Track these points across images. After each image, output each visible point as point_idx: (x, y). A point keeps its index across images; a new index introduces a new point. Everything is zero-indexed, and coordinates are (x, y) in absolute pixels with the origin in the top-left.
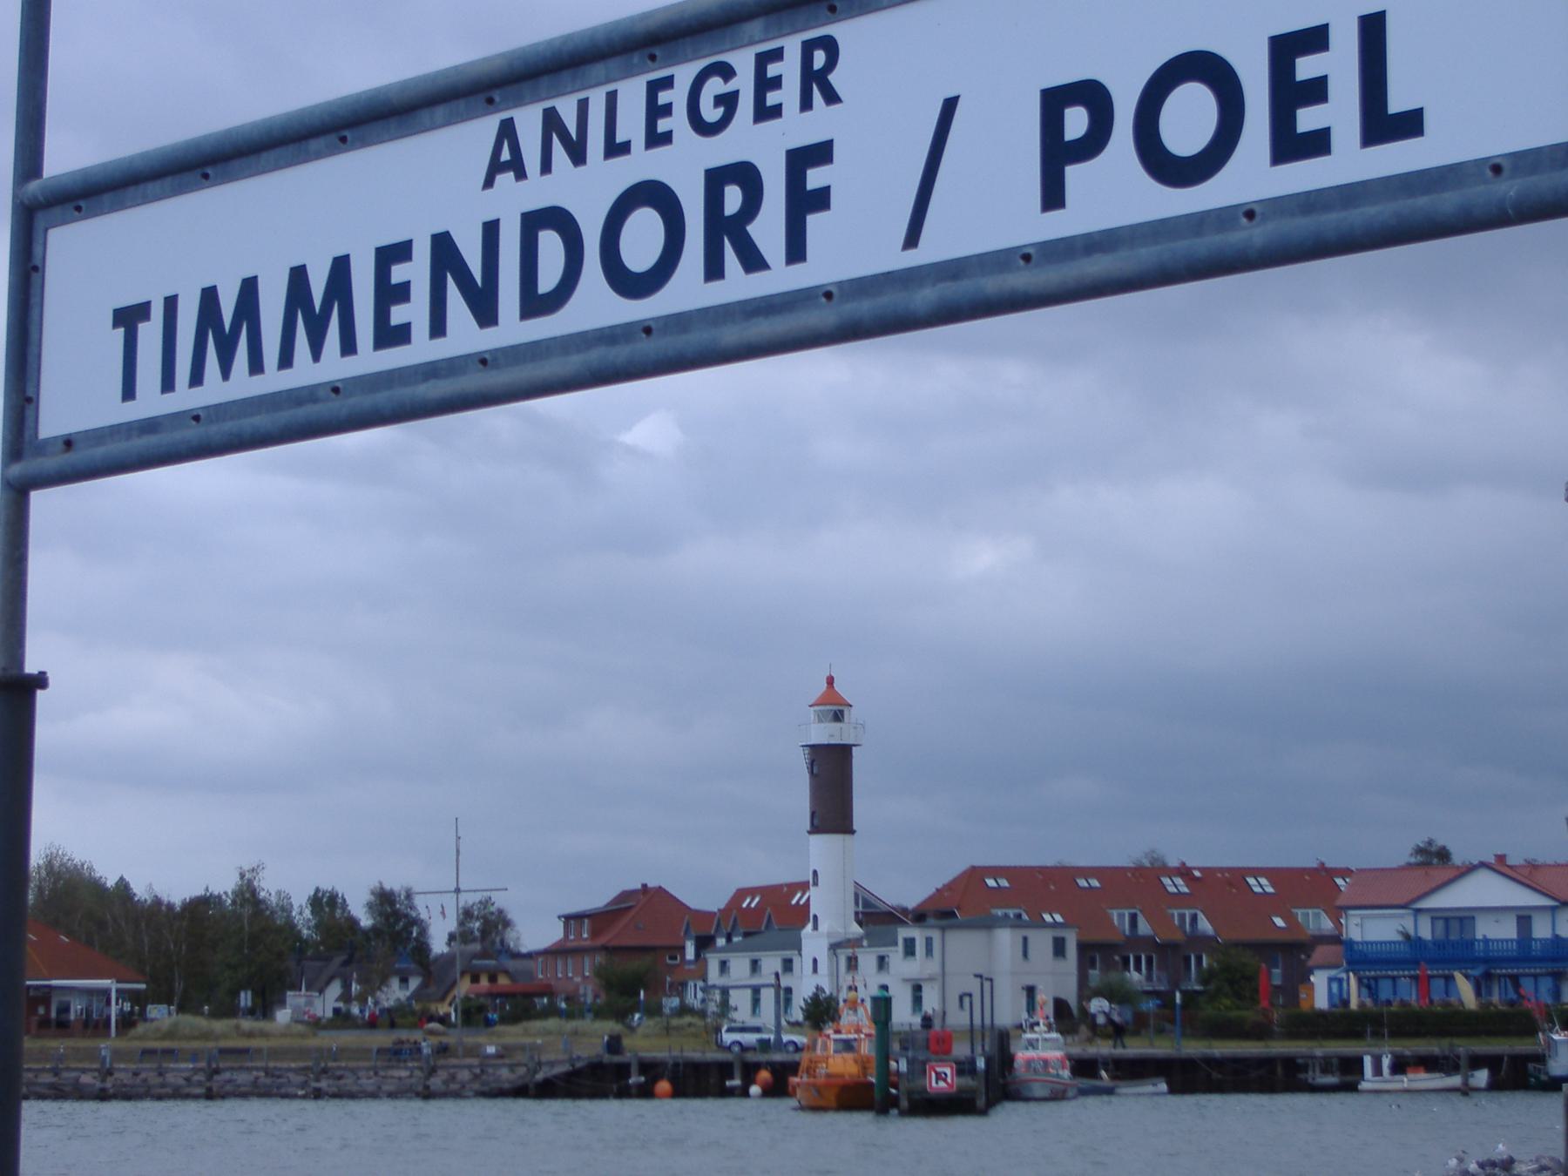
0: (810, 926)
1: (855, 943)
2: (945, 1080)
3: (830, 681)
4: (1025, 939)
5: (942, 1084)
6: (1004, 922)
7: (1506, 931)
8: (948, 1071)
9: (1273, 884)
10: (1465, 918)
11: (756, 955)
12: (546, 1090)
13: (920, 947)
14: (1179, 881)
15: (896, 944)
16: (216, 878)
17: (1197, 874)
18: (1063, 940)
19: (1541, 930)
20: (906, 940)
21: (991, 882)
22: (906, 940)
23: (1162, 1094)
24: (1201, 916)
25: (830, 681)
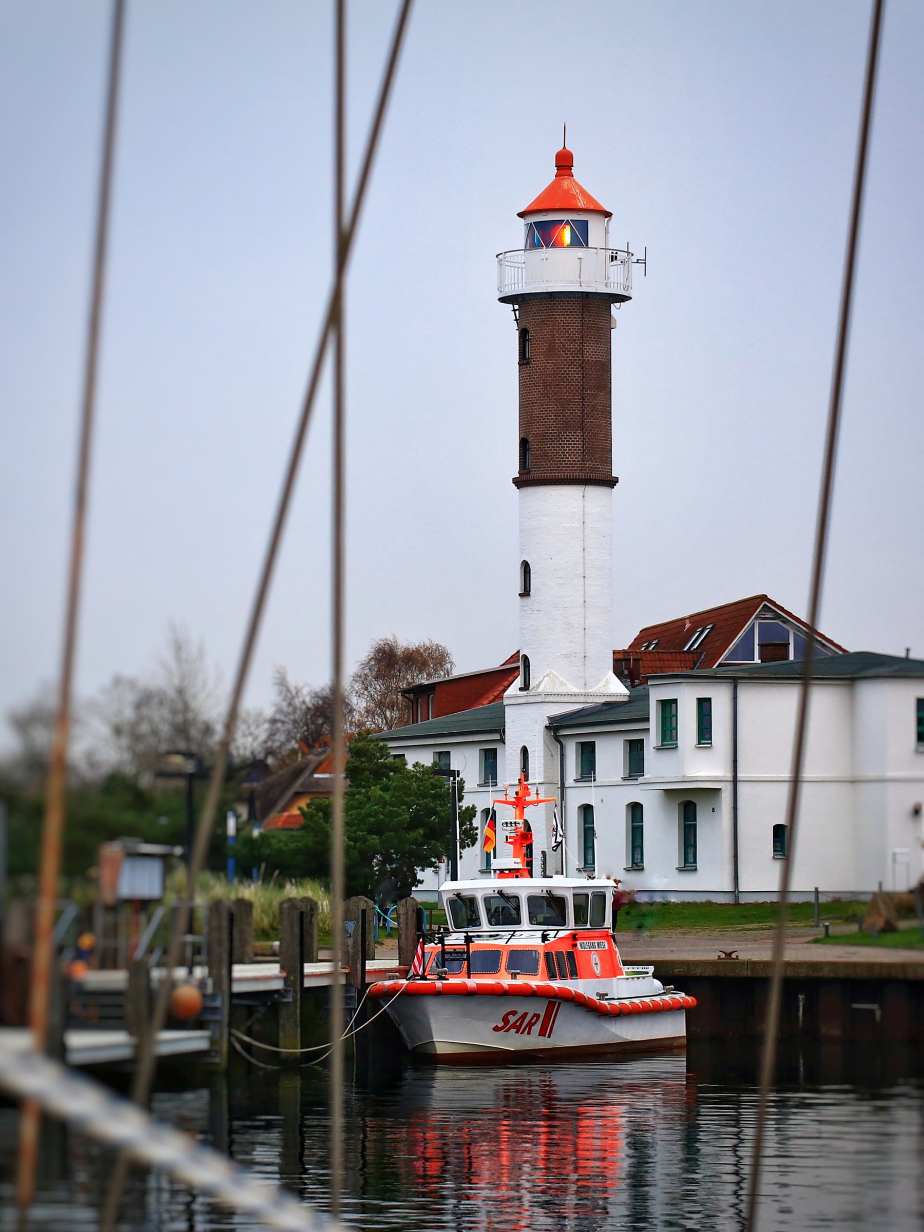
3: (564, 162)
25: (564, 162)
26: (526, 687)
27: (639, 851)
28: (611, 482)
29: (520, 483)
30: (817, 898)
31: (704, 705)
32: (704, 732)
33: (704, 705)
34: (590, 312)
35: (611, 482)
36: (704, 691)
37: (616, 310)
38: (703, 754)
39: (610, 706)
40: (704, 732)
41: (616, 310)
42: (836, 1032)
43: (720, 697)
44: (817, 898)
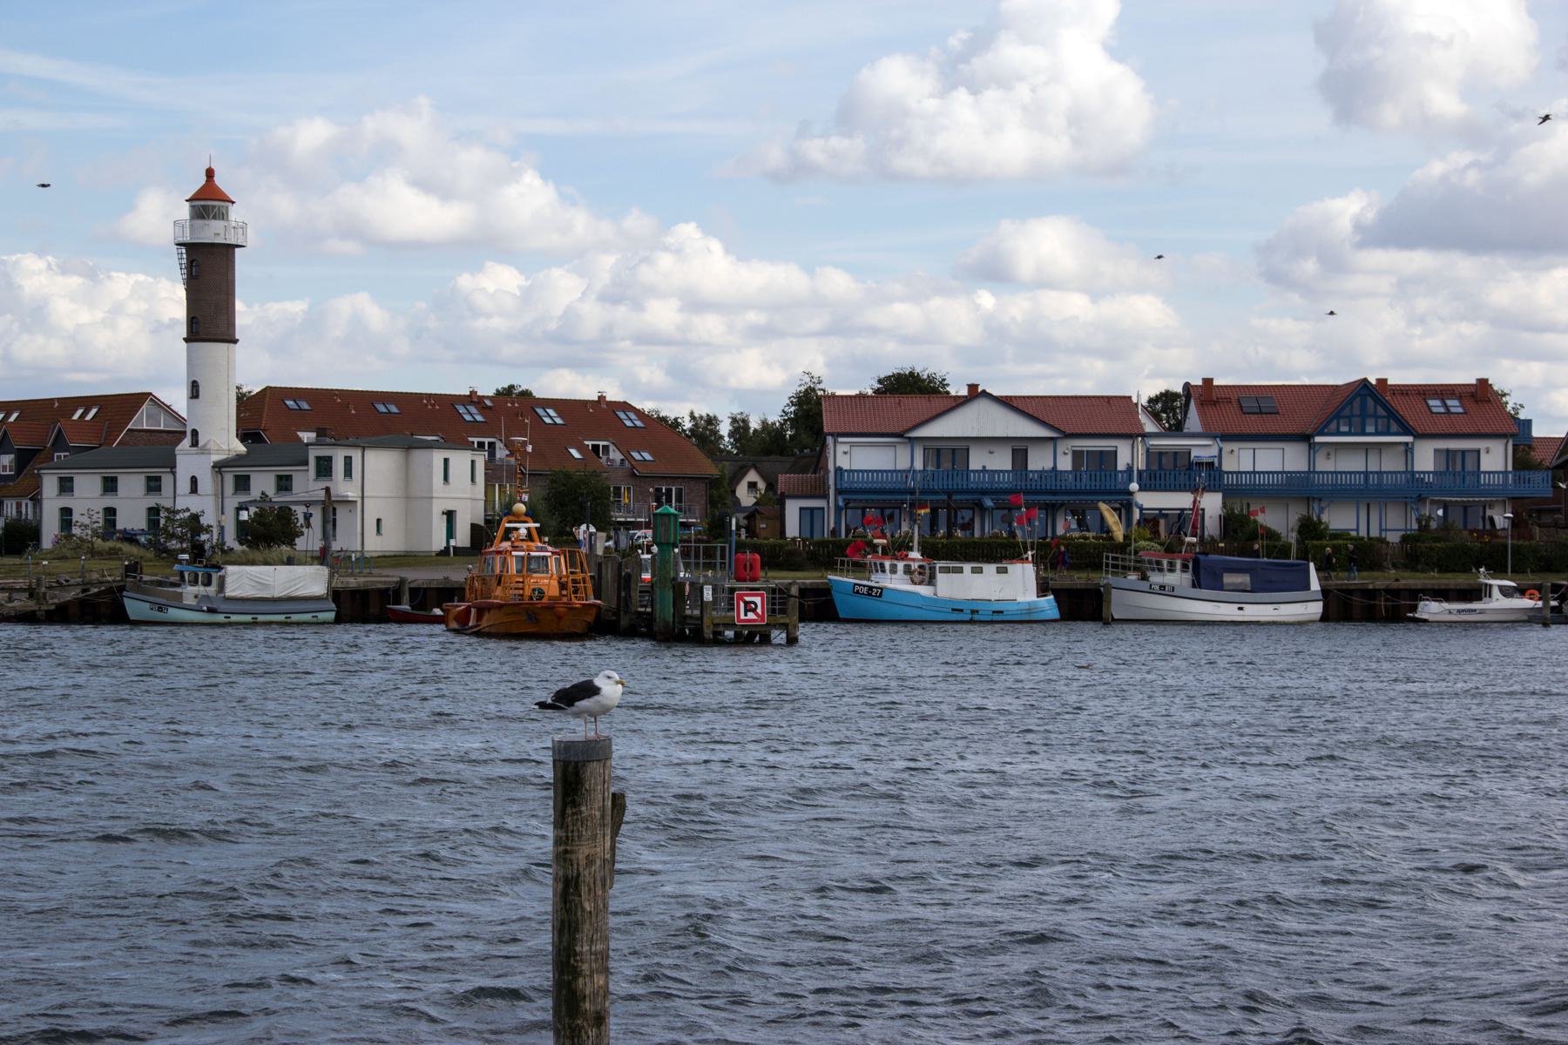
0: (187, 442)
1: (236, 461)
2: (754, 610)
3: (210, 173)
4: (446, 461)
5: (751, 616)
6: (429, 446)
7: (1001, 461)
8: (758, 600)
9: (560, 416)
10: (957, 449)
11: (110, 472)
12: (61, 615)
13: (338, 466)
14: (473, 410)
15: (306, 463)
16: (593, 396)
17: (488, 403)
18: (329, 459)
19: (1039, 461)
20: (318, 459)
21: (290, 403)
22: (318, 459)
23: (1027, 620)
24: (612, 448)
25: (210, 173)
26: (195, 443)
27: (330, 526)
28: (236, 341)
29: (186, 340)
30: (1366, 479)
31: (348, 461)
32: (348, 472)
33: (348, 461)
34: (225, 252)
35: (236, 341)
36: (349, 452)
37: (237, 250)
38: (349, 484)
39: (239, 457)
40: (348, 472)
41: (237, 250)
42: (1060, 531)
43: (356, 455)
44: (1366, 479)
